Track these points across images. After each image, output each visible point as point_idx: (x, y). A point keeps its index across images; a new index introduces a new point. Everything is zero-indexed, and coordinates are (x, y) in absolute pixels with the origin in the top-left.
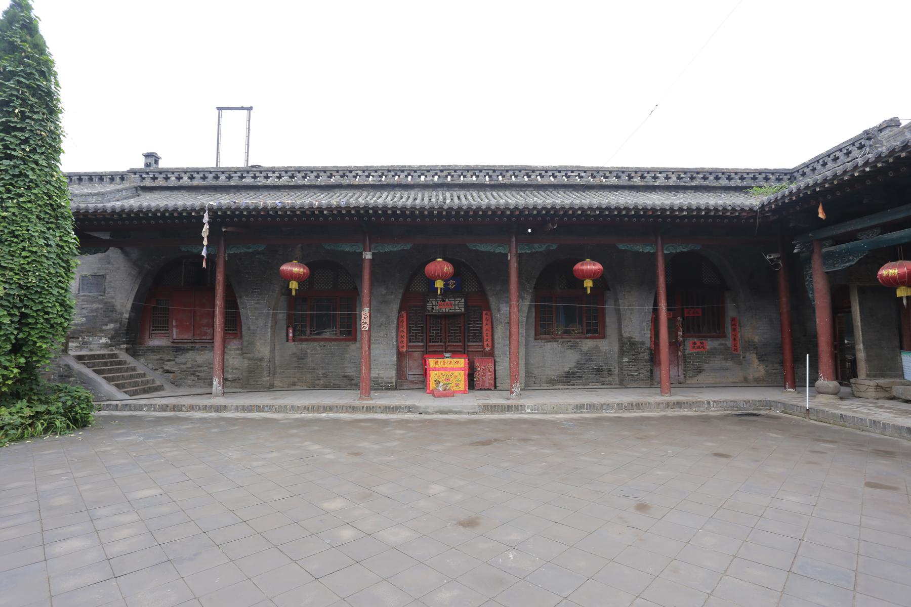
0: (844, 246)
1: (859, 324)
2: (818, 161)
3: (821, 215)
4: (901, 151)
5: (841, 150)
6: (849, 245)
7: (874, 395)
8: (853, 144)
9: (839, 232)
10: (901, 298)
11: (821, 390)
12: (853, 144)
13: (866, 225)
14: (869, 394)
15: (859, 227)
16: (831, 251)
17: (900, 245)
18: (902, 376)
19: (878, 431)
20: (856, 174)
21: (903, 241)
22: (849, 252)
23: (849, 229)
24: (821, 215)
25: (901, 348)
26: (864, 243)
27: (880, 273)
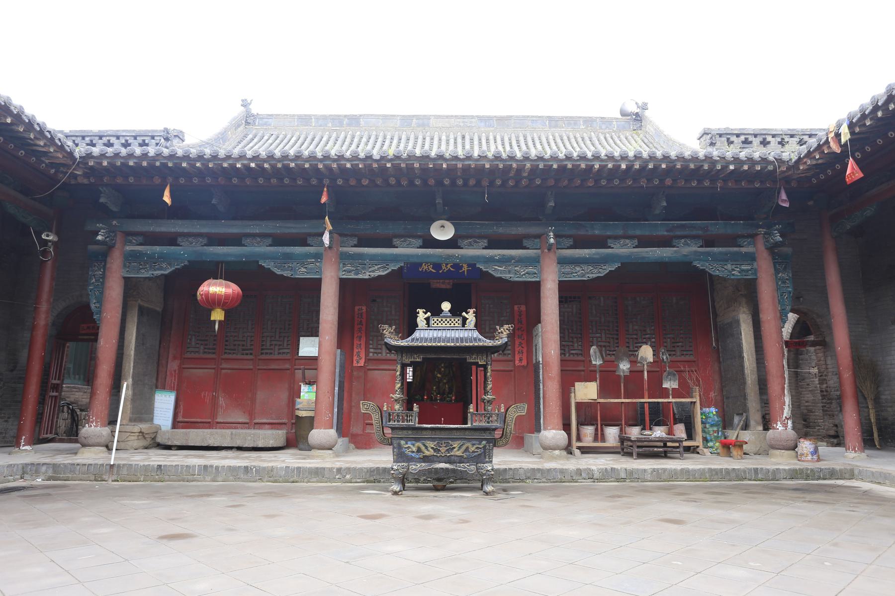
0: (158, 249)
1: (132, 353)
2: (83, 138)
3: (167, 198)
4: (292, 160)
5: (118, 138)
6: (166, 249)
7: (136, 444)
8: (135, 138)
9: (158, 229)
10: (215, 321)
11: (90, 441)
12: (135, 138)
13: (195, 231)
14: (130, 443)
15: (186, 231)
16: (139, 252)
17: (222, 262)
18: (152, 420)
19: (208, 478)
20: (239, 166)
21: (229, 259)
22: (163, 257)
23: (173, 230)
24: (167, 198)
25: (157, 387)
26: (186, 252)
27: (201, 289)
